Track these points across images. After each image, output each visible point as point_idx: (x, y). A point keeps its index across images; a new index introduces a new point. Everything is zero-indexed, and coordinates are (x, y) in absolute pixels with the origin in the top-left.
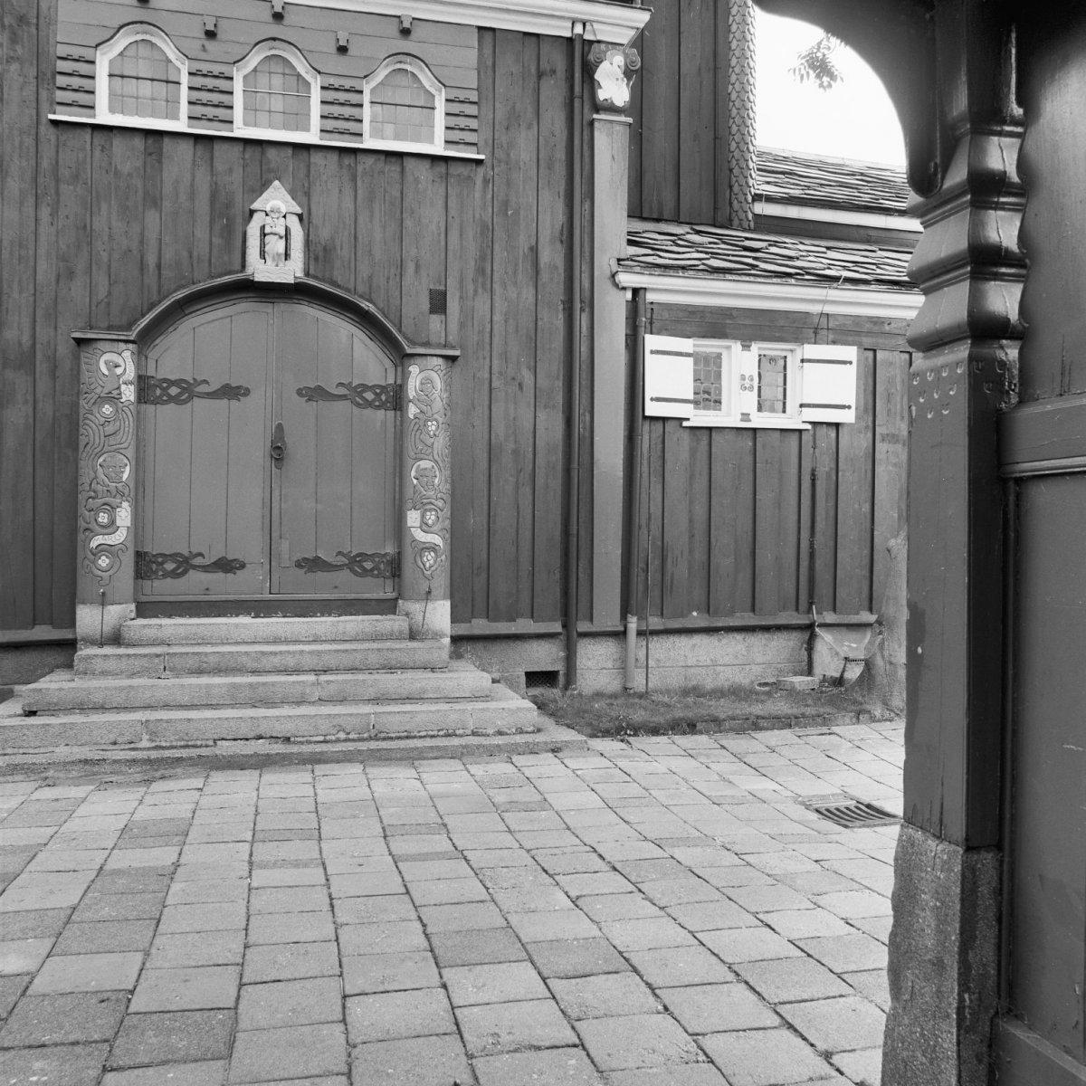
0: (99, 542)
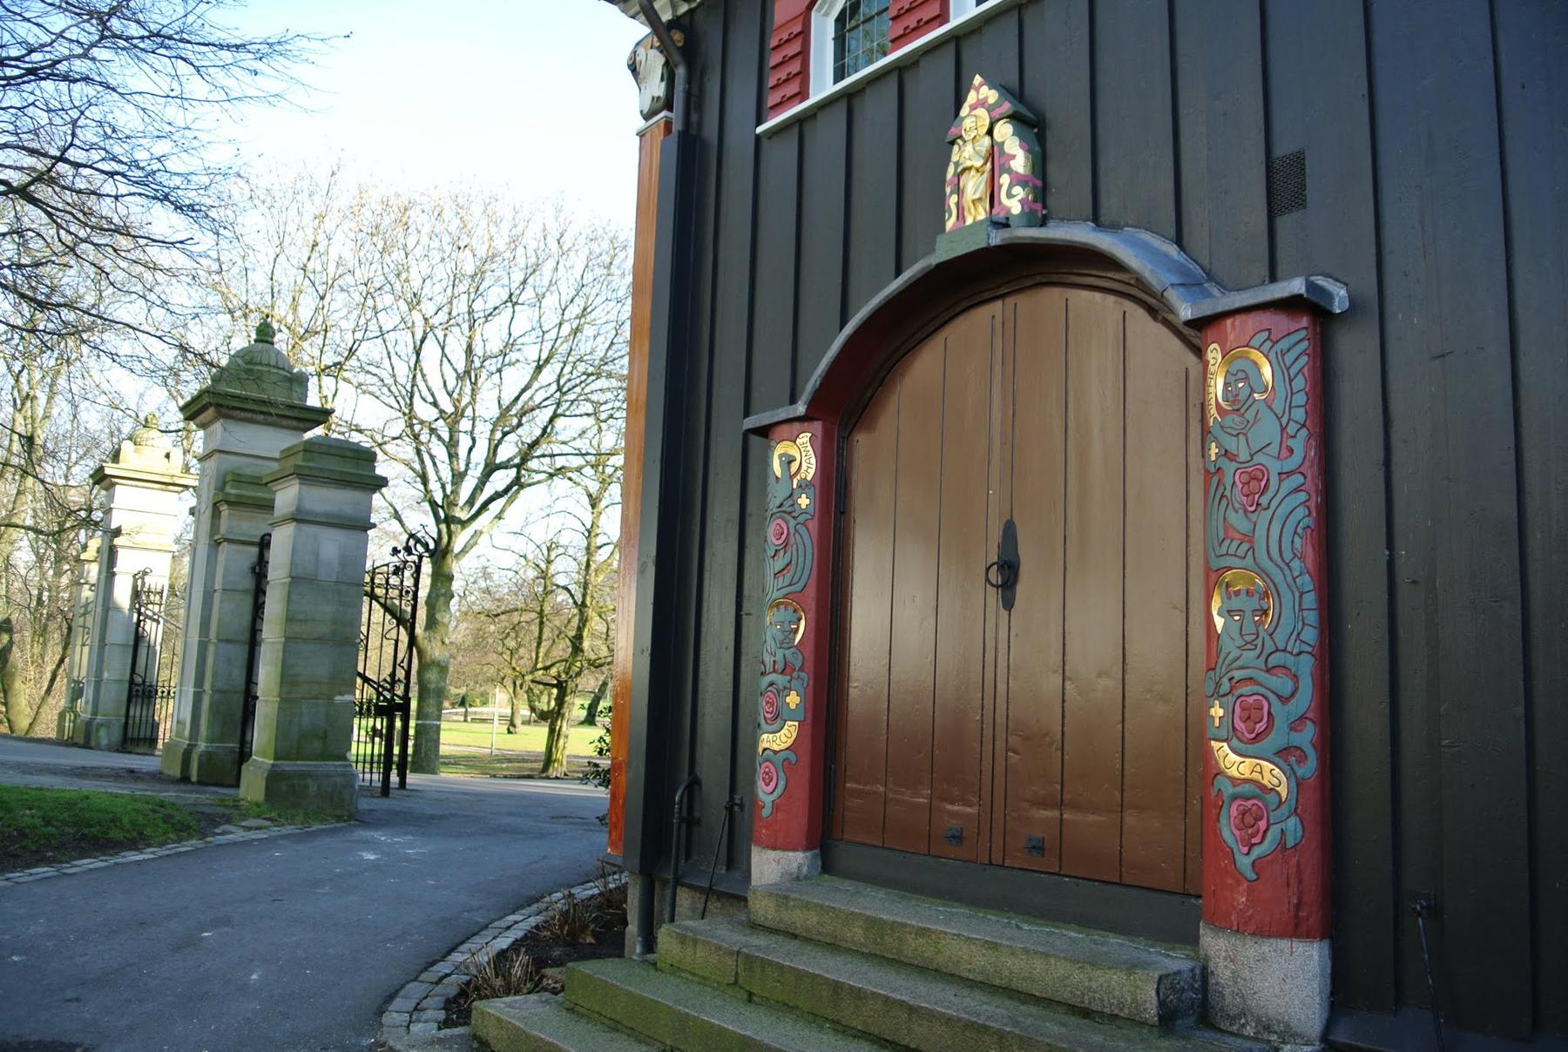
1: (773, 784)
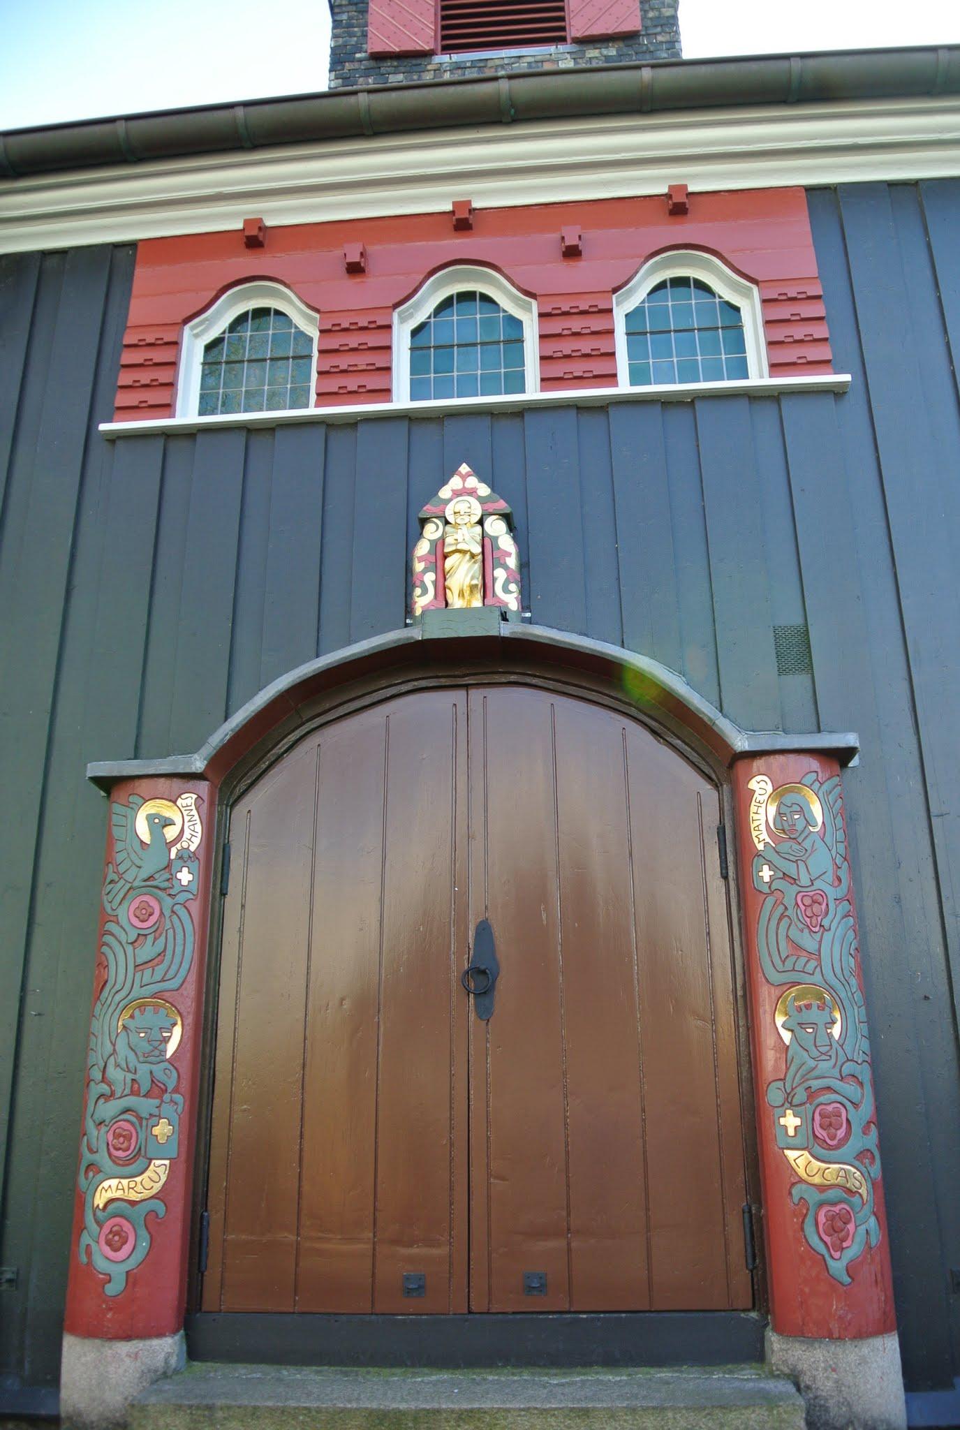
0: (110, 1195)
1: (127, 1248)
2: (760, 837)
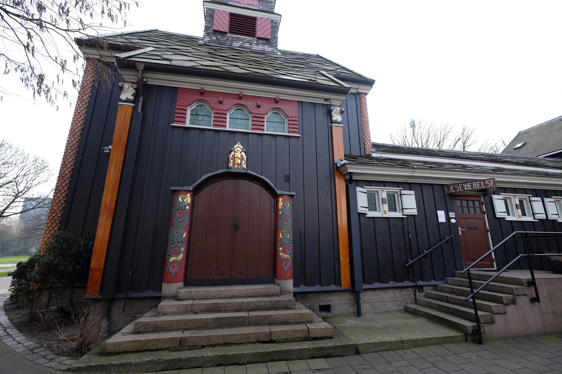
2: (280, 207)
